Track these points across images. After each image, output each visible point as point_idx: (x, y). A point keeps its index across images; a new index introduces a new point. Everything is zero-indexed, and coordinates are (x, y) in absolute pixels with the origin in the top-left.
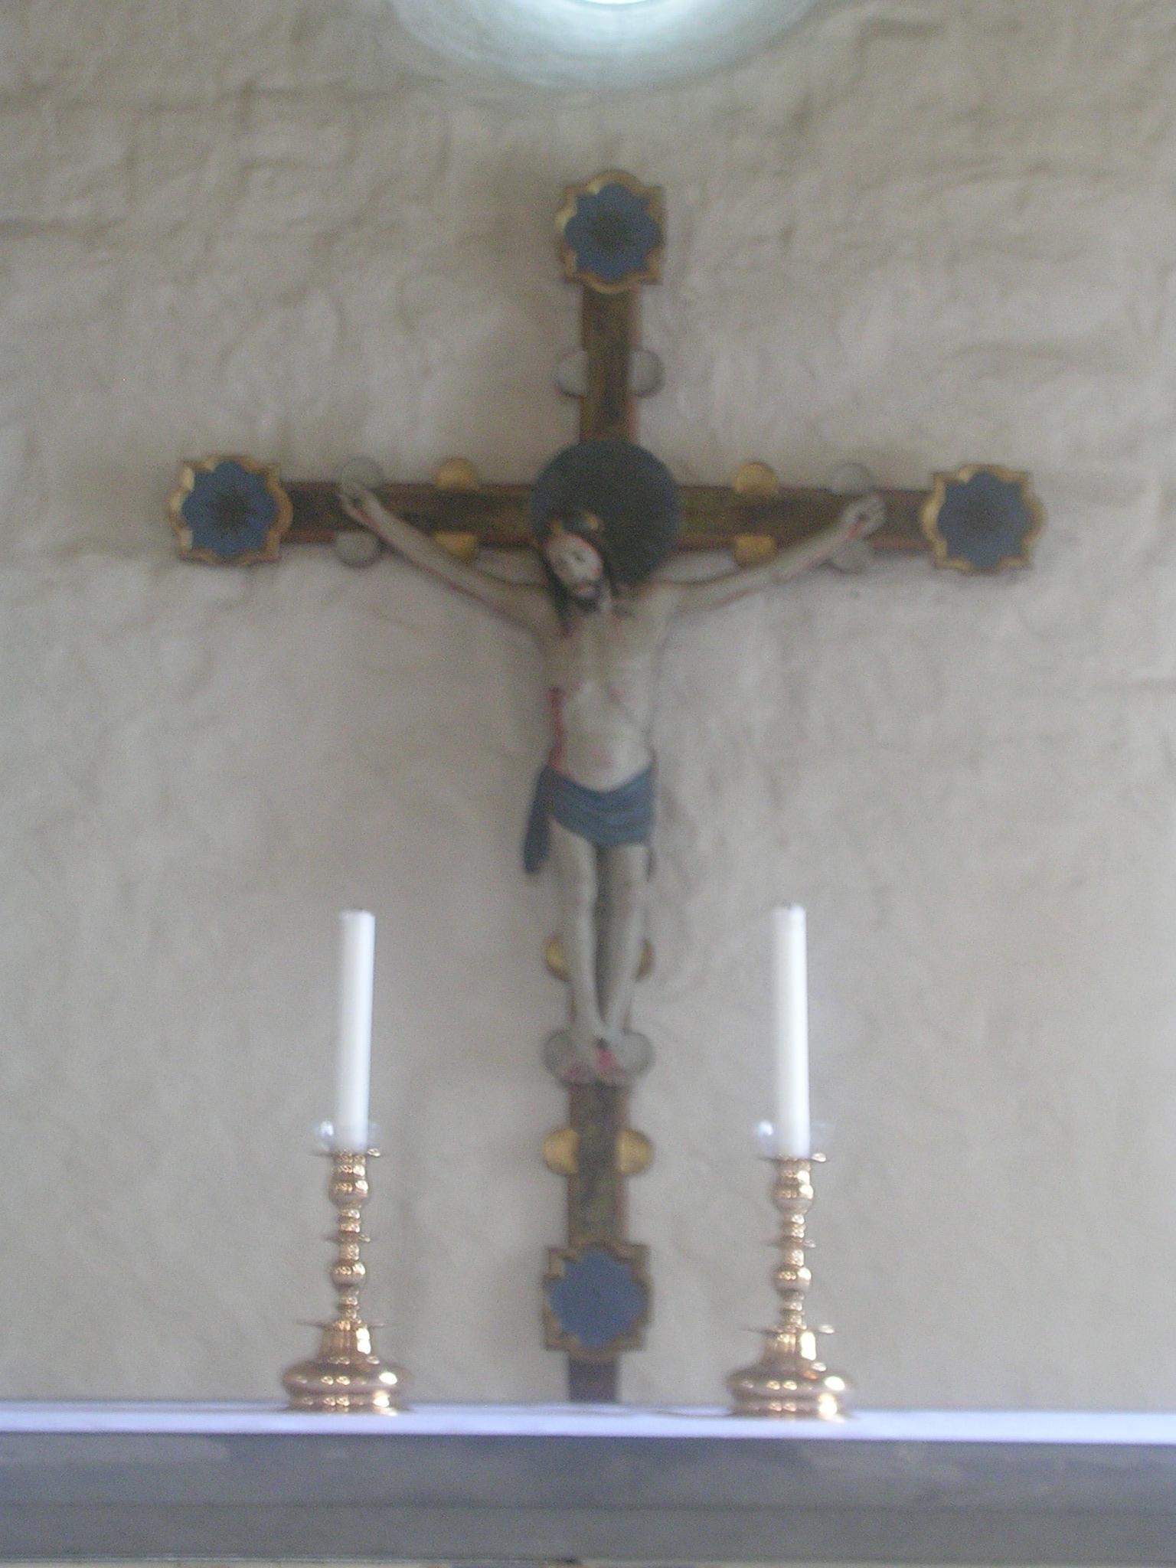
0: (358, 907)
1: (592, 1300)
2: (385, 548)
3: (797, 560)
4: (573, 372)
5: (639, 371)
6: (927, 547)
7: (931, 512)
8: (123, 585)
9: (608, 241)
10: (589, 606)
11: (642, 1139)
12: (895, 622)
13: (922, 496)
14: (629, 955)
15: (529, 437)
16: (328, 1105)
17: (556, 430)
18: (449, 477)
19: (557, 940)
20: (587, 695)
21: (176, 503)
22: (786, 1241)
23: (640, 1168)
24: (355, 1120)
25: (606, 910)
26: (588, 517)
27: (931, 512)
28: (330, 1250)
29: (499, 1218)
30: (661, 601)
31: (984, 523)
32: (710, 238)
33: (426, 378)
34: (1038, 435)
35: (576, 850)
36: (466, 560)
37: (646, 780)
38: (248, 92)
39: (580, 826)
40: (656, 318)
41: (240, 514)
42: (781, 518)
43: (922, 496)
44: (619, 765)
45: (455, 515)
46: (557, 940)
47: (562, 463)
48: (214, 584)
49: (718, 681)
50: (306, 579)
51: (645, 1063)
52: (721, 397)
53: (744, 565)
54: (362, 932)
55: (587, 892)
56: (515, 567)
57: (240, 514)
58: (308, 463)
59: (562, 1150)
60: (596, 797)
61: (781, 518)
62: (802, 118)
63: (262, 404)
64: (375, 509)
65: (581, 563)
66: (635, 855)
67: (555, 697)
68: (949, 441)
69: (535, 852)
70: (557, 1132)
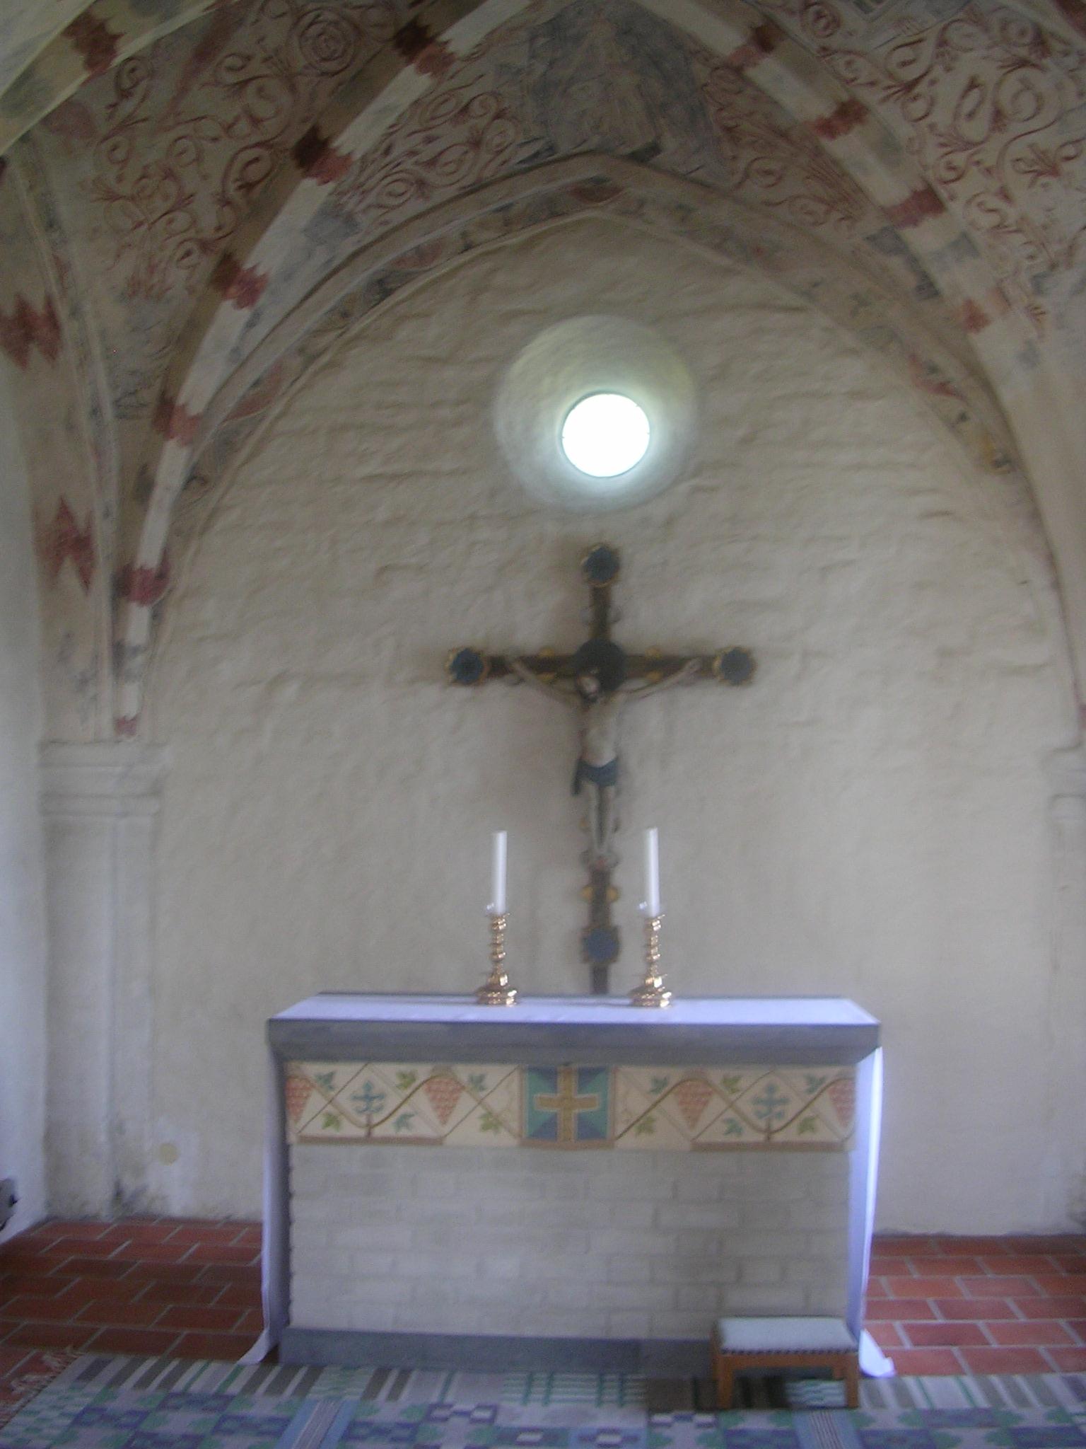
0: (501, 829)
1: (599, 948)
2: (521, 680)
3: (680, 676)
4: (589, 615)
5: (612, 614)
6: (714, 676)
7: (717, 664)
8: (431, 693)
9: (601, 567)
10: (594, 700)
11: (616, 889)
12: (702, 704)
13: (714, 658)
14: (610, 824)
15: (575, 638)
16: (489, 897)
17: (582, 636)
18: (545, 654)
19: (585, 820)
20: (593, 732)
21: (448, 665)
22: (649, 946)
23: (616, 899)
24: (499, 902)
25: (602, 809)
26: (595, 667)
27: (717, 664)
28: (491, 950)
29: (565, 916)
30: (620, 698)
31: (736, 667)
32: (639, 564)
33: (535, 617)
34: (755, 633)
35: (591, 788)
36: (551, 683)
37: (617, 759)
38: (473, 517)
39: (593, 778)
40: (619, 594)
41: (472, 667)
42: (665, 667)
43: (714, 658)
44: (606, 757)
45: (545, 667)
46: (585, 820)
47: (585, 648)
48: (463, 692)
49: (646, 726)
50: (495, 691)
51: (616, 863)
52: (643, 622)
53: (653, 683)
54: (501, 840)
55: (594, 803)
56: (568, 685)
57: (472, 667)
58: (495, 648)
59: (588, 892)
60: (596, 769)
61: (665, 667)
62: (670, 522)
63: (477, 627)
64: (517, 666)
65: (591, 685)
66: (611, 790)
67: (583, 733)
68: (726, 637)
69: (577, 788)
70: (585, 887)
